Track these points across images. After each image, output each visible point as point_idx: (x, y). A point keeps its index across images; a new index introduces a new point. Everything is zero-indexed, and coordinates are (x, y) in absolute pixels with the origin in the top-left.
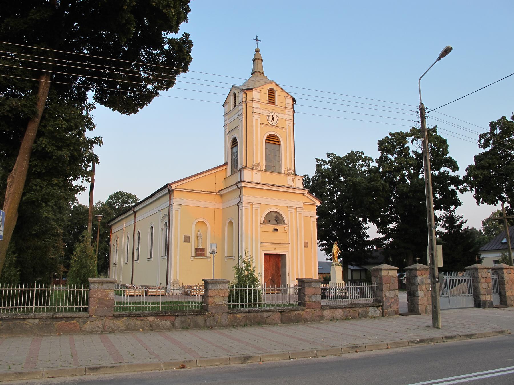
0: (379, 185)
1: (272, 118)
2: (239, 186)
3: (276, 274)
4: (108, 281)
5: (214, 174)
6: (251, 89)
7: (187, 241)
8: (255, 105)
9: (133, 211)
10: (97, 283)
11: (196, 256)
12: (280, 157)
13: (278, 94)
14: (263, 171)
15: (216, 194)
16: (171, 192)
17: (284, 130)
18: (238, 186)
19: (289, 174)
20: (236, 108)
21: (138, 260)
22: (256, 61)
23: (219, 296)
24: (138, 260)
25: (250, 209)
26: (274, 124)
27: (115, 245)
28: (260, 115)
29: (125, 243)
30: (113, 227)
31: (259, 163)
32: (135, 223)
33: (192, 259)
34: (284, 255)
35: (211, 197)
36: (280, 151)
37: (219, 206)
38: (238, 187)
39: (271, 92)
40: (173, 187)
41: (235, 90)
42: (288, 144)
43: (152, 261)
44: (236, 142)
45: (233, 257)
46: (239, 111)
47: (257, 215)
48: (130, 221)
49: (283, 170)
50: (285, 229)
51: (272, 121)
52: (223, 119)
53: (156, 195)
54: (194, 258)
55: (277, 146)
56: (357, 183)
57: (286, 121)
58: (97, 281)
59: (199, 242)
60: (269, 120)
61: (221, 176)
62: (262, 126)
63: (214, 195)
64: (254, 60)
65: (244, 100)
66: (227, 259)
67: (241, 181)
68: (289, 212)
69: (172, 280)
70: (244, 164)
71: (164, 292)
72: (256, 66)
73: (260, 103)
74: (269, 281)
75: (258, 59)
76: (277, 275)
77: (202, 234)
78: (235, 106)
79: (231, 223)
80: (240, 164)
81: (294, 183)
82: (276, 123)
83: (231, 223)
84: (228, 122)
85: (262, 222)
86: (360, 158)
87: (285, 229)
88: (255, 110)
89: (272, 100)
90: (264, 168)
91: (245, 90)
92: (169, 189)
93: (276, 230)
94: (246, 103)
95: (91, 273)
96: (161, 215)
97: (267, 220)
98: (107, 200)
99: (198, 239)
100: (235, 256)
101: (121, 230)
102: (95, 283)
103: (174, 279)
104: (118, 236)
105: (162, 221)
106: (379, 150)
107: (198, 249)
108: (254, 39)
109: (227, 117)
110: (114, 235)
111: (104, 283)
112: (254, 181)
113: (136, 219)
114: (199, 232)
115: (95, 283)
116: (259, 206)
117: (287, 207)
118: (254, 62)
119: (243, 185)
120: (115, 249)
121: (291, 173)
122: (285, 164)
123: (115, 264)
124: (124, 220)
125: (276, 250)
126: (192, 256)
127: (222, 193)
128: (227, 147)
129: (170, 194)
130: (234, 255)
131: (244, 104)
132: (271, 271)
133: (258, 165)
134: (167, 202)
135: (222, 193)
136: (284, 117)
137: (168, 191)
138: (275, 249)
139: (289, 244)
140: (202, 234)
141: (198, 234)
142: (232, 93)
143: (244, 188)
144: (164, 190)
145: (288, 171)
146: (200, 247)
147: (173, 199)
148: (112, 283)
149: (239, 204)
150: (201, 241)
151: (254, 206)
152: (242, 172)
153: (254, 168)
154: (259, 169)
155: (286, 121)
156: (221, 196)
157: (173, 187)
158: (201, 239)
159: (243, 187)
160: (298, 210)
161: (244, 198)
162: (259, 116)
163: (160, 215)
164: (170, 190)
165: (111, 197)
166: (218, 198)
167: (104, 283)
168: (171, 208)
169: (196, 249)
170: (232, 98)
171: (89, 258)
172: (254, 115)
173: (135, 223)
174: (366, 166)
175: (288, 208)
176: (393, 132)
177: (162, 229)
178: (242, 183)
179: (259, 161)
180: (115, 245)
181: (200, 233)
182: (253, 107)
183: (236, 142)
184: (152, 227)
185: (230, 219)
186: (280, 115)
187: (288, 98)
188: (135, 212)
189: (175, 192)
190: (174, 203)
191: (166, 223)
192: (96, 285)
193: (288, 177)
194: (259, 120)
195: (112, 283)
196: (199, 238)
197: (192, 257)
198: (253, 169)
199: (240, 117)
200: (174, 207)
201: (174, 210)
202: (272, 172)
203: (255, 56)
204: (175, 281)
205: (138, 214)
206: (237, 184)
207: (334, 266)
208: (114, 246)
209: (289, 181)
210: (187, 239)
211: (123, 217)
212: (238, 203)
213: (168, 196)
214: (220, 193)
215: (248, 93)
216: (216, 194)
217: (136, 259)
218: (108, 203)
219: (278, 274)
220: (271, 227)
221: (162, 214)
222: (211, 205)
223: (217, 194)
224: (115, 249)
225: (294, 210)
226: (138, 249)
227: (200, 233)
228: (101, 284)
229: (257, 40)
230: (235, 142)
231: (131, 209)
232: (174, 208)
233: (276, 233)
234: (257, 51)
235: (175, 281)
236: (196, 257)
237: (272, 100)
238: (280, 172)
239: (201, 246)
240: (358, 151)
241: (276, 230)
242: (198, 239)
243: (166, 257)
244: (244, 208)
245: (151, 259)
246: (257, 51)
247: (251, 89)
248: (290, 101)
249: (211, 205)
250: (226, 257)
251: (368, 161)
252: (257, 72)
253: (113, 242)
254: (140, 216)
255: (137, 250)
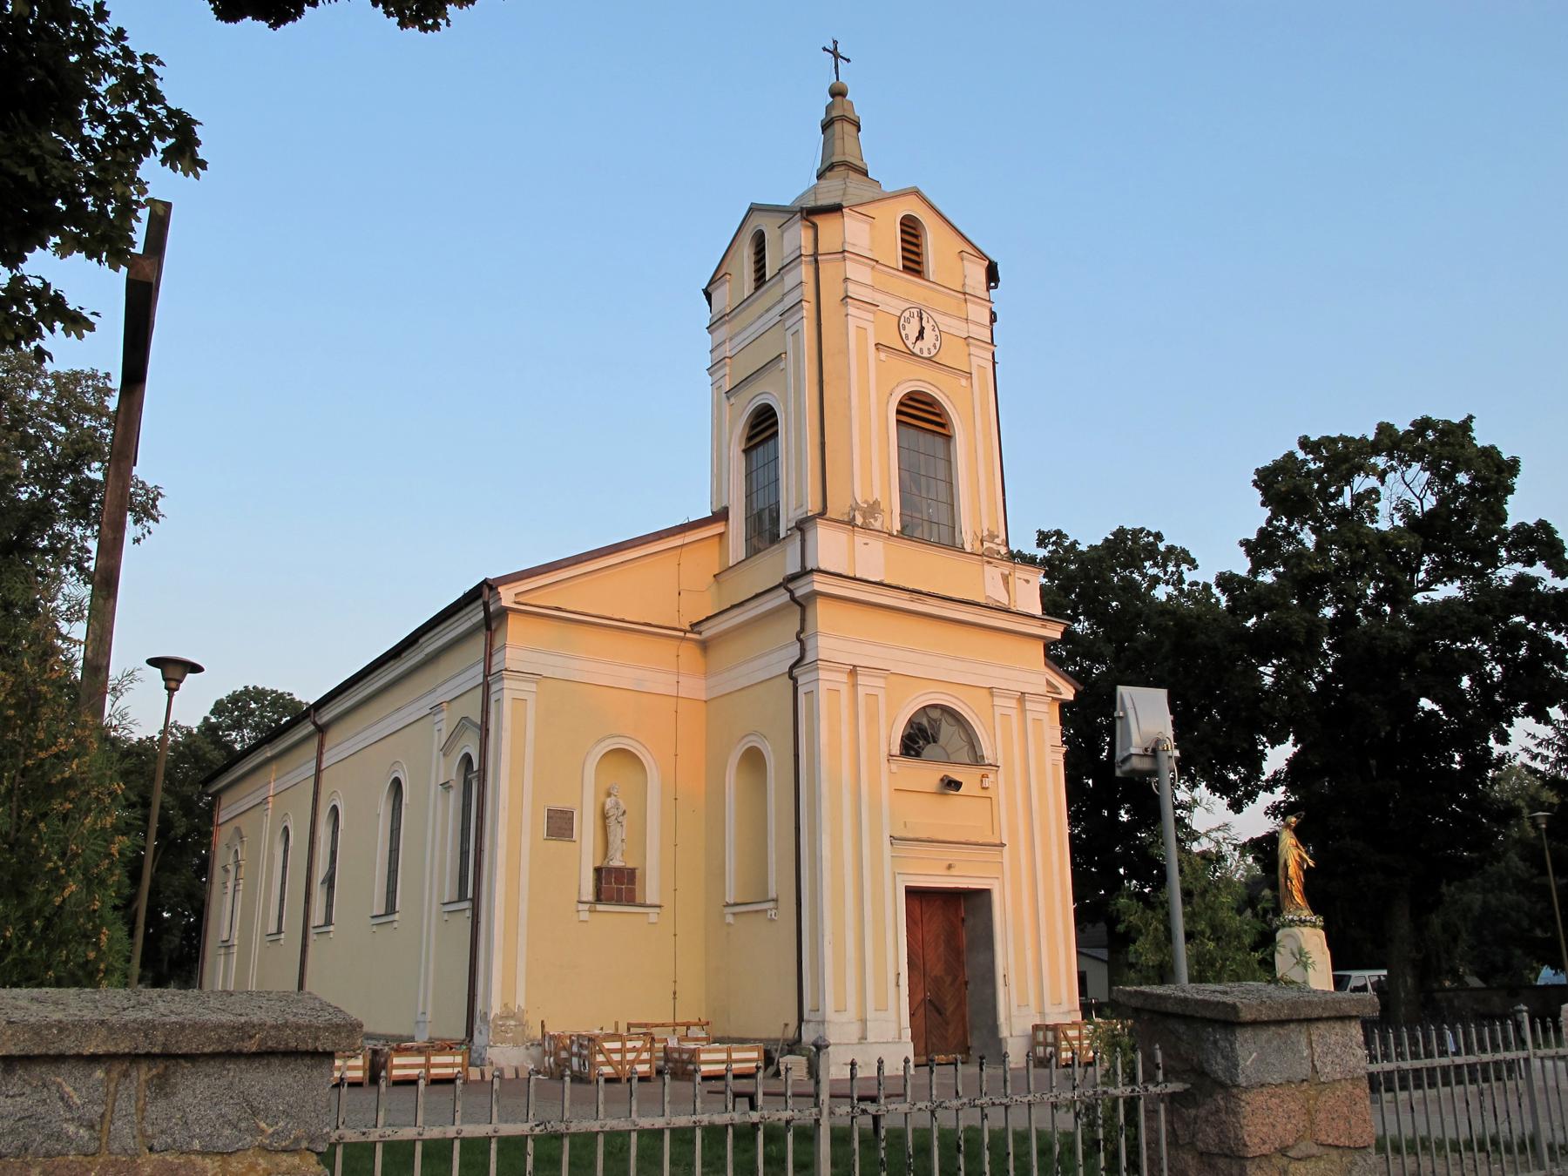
0: (1297, 623)
1: (917, 328)
2: (798, 593)
3: (948, 980)
4: (244, 1030)
5: (674, 552)
6: (836, 209)
7: (563, 835)
8: (854, 270)
9: (314, 723)
10: (94, 1059)
11: (599, 899)
12: (950, 484)
13: (935, 242)
14: (891, 535)
15: (683, 639)
16: (493, 621)
17: (964, 382)
18: (791, 591)
19: (988, 557)
20: (766, 291)
21: (328, 922)
22: (837, 126)
23: (1315, 1150)
24: (328, 922)
25: (845, 690)
26: (926, 354)
27: (231, 868)
28: (874, 313)
29: (271, 857)
30: (225, 800)
31: (876, 503)
32: (319, 771)
33: (585, 916)
34: (986, 893)
35: (667, 649)
36: (949, 461)
37: (695, 687)
38: (793, 598)
39: (911, 230)
40: (507, 596)
41: (759, 222)
42: (979, 436)
43: (395, 925)
44: (770, 422)
45: (771, 905)
46: (784, 295)
47: (873, 718)
48: (300, 768)
49: (969, 543)
50: (987, 783)
51: (917, 339)
52: (707, 340)
53: (421, 641)
54: (590, 911)
55: (939, 440)
56: (1194, 621)
57: (968, 345)
58: (86, 1028)
59: (611, 838)
60: (907, 335)
61: (701, 562)
62: (883, 356)
63: (676, 643)
64: (827, 126)
65: (808, 249)
66: (734, 914)
67: (805, 572)
68: (998, 711)
69: (496, 1009)
70: (813, 506)
71: (462, 1065)
72: (838, 143)
73: (873, 268)
74: (922, 1010)
75: (843, 118)
76: (952, 984)
77: (623, 806)
78: (760, 279)
79: (754, 759)
80: (793, 504)
81: (1008, 592)
82: (934, 352)
83: (754, 759)
84: (727, 350)
85: (896, 750)
86: (1151, 552)
87: (987, 783)
88: (853, 290)
89: (913, 263)
90: (897, 526)
91: (811, 213)
92: (486, 606)
93: (952, 785)
94: (816, 261)
95: (62, 942)
96: (443, 725)
97: (917, 740)
98: (206, 719)
99: (605, 828)
100: (775, 900)
101: (258, 809)
102: (60, 1058)
103: (506, 1005)
104: (244, 833)
105: (446, 750)
106: (1263, 504)
107: (610, 870)
108: (825, 49)
109: (723, 332)
110: (229, 828)
111: (190, 1057)
112: (858, 576)
113: (325, 757)
114: (609, 795)
115: (60, 1058)
116: (880, 682)
117: (985, 692)
118: (829, 131)
119: (817, 587)
120: (230, 884)
121: (999, 553)
122: (971, 522)
123: (227, 945)
124: (274, 766)
125: (953, 872)
126: (584, 899)
127: (709, 631)
128: (725, 450)
129: (488, 628)
130: (772, 895)
131: (805, 272)
132: (928, 967)
133: (873, 509)
134: (472, 666)
135: (709, 631)
136: (961, 329)
137: (482, 614)
138: (950, 867)
139: (1003, 845)
140: (623, 806)
141: (607, 807)
142: (747, 238)
143: (820, 602)
144: (463, 612)
145: (986, 545)
146: (617, 862)
147: (504, 647)
148: (291, 1054)
149: (796, 672)
150: (617, 834)
151: (861, 680)
152: (809, 536)
153: (859, 521)
154: (877, 525)
155: (968, 345)
156: (704, 646)
157: (507, 596)
158: (619, 829)
159: (816, 594)
160: (1028, 706)
161: (822, 641)
162: (870, 317)
163: (437, 727)
164: (492, 609)
165: (219, 708)
166: (689, 653)
167: (190, 1057)
168: (494, 688)
169: (598, 871)
170: (747, 253)
171: (57, 805)
172: (851, 310)
173: (319, 771)
174: (1167, 583)
175: (992, 694)
176: (1314, 438)
177: (446, 786)
178: (816, 577)
179: (877, 495)
180: (231, 868)
181: (617, 803)
182: (846, 279)
183: (770, 422)
184: (397, 783)
185: (751, 738)
186: (945, 323)
187: (970, 261)
188: (321, 730)
189: (511, 617)
190: (509, 664)
191: (467, 759)
192: (72, 1085)
193: (987, 567)
194: (871, 329)
195: (291, 1054)
196: (612, 822)
197: (581, 907)
198: (851, 523)
199: (788, 318)
200: (507, 683)
201: (507, 696)
202: (923, 541)
203: (829, 108)
204: (507, 1015)
205: (332, 737)
206: (791, 586)
207: (1296, 930)
208: (227, 871)
209: (990, 583)
210: (560, 824)
211: (269, 754)
212: (792, 667)
213: (480, 642)
214: (700, 633)
215: (826, 224)
216: (683, 639)
217: (317, 917)
218: (208, 729)
219: (955, 978)
220: (926, 774)
221: (445, 723)
222: (661, 682)
223: (688, 635)
224: (230, 884)
225: (1013, 703)
226: (330, 881)
227: (617, 803)
228: (143, 1073)
229: (835, 54)
230: (763, 425)
231: (304, 718)
232: (509, 691)
233: (954, 800)
234: (838, 93)
235: (507, 1015)
236: (600, 907)
237: (913, 263)
238: (954, 546)
239: (618, 855)
240: (1142, 530)
241: (952, 785)
242: (605, 828)
243: (466, 905)
244: (823, 686)
245: (391, 918)
246: (838, 93)
247: (836, 209)
248: (978, 273)
249: (661, 682)
250: (728, 905)
251: (1177, 566)
252: (845, 164)
253: (222, 857)
254: (340, 746)
255: (323, 883)
